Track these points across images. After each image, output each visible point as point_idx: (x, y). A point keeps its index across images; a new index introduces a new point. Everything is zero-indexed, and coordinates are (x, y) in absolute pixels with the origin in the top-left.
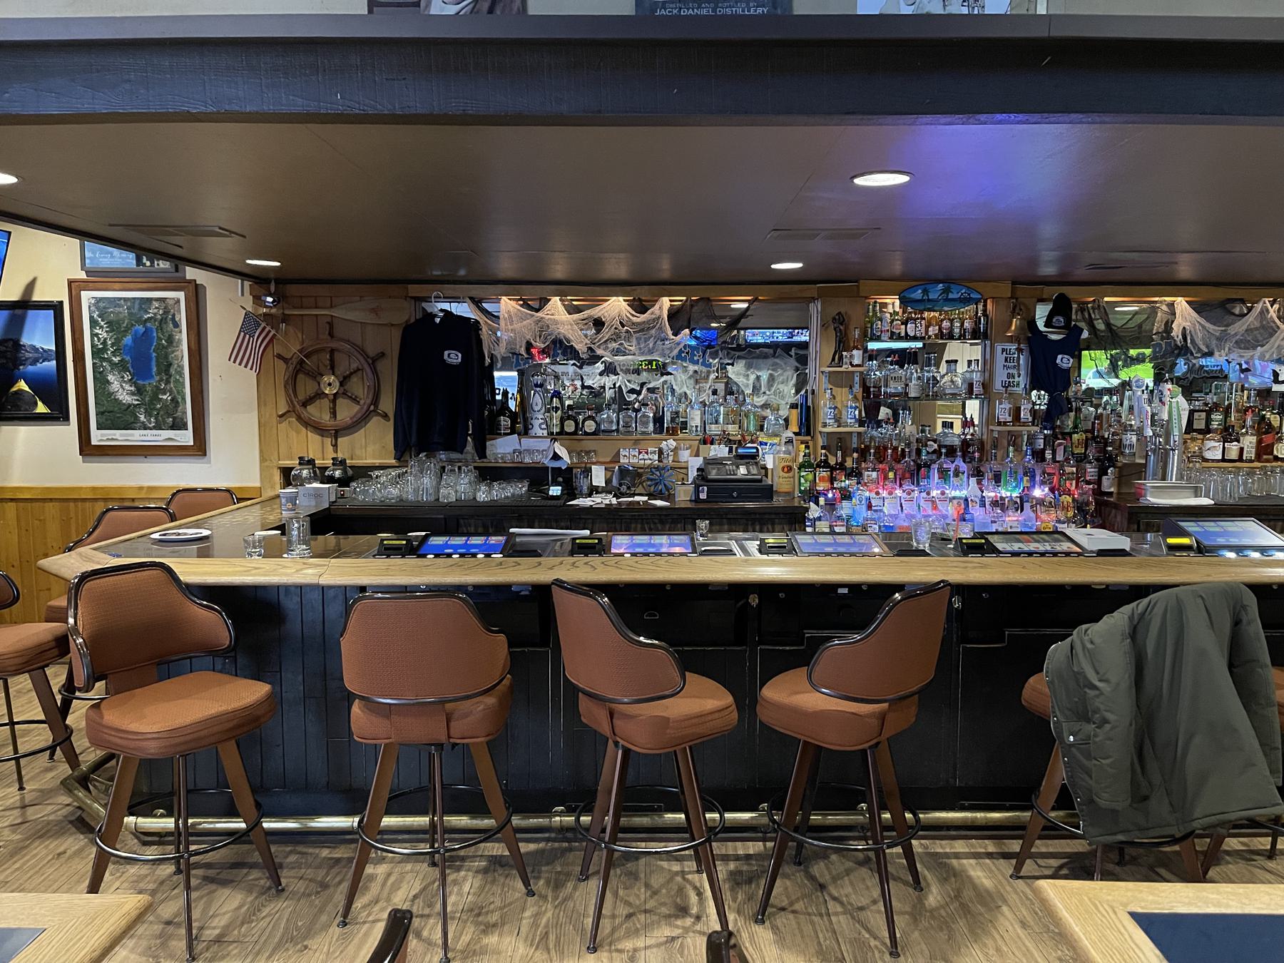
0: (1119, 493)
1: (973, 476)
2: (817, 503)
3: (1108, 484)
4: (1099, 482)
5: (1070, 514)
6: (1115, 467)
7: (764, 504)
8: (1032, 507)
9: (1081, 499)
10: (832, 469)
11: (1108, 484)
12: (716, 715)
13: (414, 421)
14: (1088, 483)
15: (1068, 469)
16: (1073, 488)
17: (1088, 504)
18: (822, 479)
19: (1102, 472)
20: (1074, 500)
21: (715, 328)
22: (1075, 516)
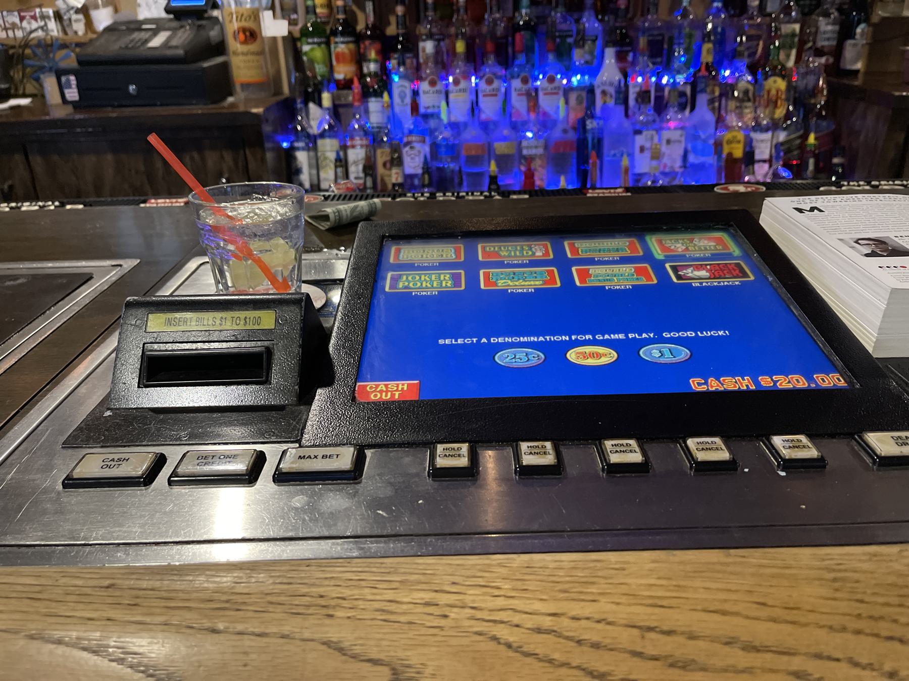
0: (867, 73)
1: (614, 44)
2: (319, 104)
3: (855, 60)
4: (837, 52)
5: (780, 113)
6: (867, 20)
7: (210, 109)
8: (711, 101)
9: (801, 85)
10: (358, 38)
11: (855, 60)
12: (175, 443)
13: (237, 297)
14: (819, 53)
15: (786, 28)
16: (791, 64)
17: (815, 91)
18: (340, 58)
19: (846, 32)
20: (789, 87)
21: (24, 96)
22: (788, 115)
